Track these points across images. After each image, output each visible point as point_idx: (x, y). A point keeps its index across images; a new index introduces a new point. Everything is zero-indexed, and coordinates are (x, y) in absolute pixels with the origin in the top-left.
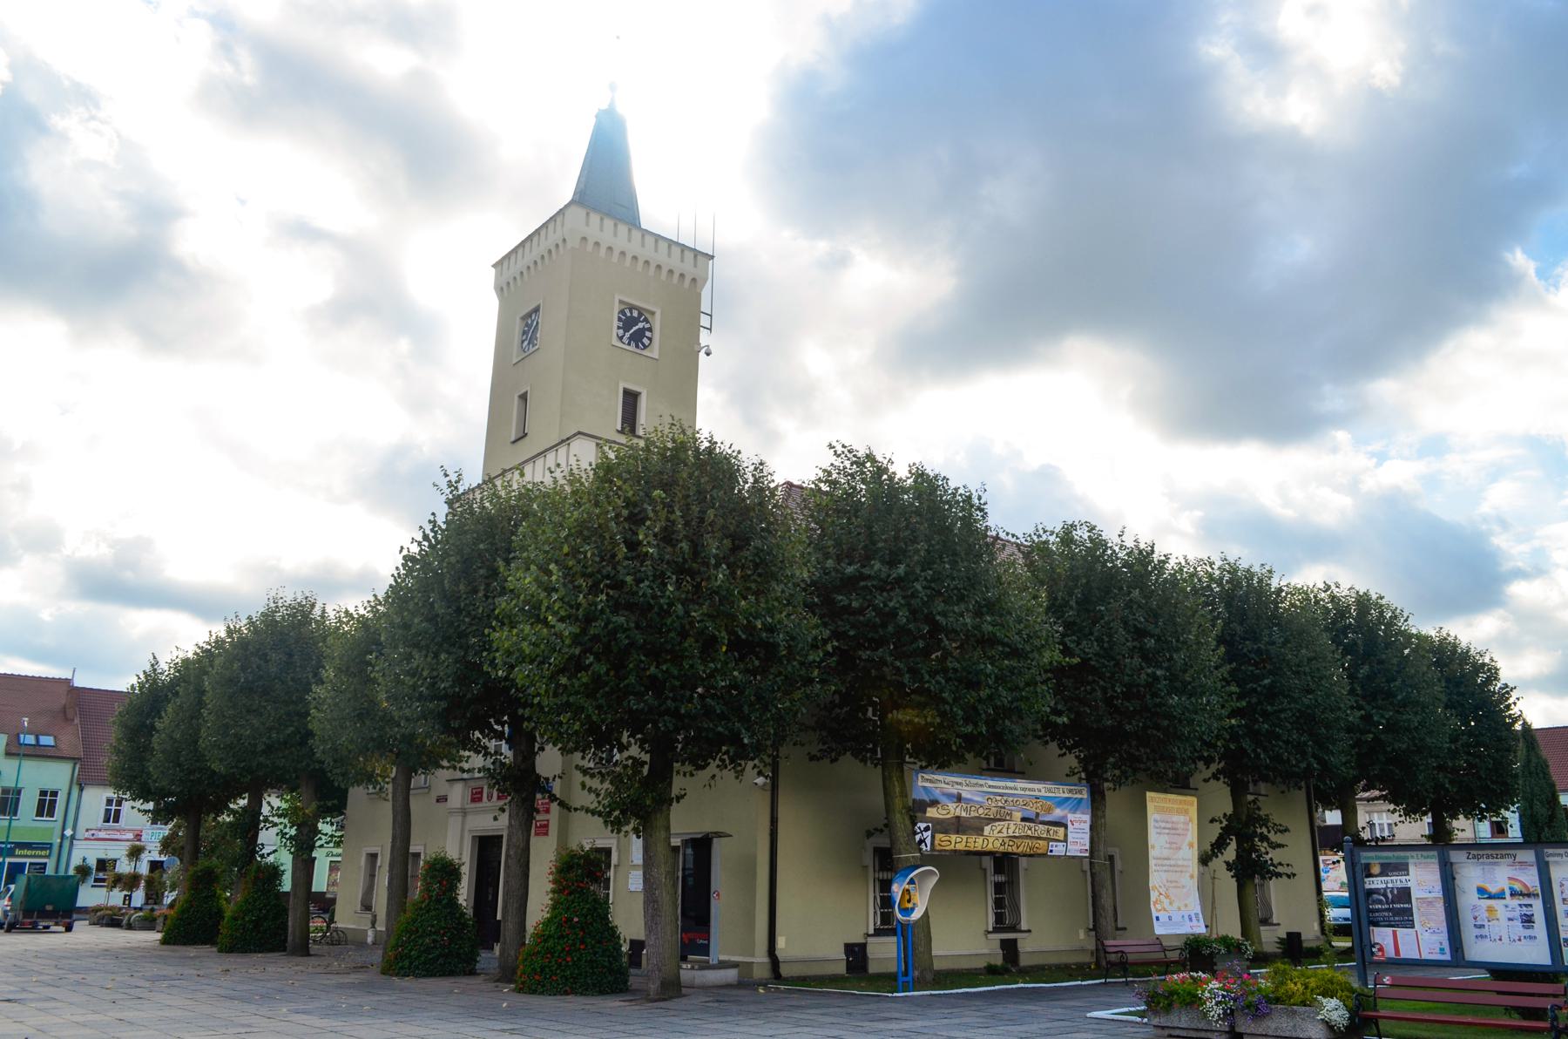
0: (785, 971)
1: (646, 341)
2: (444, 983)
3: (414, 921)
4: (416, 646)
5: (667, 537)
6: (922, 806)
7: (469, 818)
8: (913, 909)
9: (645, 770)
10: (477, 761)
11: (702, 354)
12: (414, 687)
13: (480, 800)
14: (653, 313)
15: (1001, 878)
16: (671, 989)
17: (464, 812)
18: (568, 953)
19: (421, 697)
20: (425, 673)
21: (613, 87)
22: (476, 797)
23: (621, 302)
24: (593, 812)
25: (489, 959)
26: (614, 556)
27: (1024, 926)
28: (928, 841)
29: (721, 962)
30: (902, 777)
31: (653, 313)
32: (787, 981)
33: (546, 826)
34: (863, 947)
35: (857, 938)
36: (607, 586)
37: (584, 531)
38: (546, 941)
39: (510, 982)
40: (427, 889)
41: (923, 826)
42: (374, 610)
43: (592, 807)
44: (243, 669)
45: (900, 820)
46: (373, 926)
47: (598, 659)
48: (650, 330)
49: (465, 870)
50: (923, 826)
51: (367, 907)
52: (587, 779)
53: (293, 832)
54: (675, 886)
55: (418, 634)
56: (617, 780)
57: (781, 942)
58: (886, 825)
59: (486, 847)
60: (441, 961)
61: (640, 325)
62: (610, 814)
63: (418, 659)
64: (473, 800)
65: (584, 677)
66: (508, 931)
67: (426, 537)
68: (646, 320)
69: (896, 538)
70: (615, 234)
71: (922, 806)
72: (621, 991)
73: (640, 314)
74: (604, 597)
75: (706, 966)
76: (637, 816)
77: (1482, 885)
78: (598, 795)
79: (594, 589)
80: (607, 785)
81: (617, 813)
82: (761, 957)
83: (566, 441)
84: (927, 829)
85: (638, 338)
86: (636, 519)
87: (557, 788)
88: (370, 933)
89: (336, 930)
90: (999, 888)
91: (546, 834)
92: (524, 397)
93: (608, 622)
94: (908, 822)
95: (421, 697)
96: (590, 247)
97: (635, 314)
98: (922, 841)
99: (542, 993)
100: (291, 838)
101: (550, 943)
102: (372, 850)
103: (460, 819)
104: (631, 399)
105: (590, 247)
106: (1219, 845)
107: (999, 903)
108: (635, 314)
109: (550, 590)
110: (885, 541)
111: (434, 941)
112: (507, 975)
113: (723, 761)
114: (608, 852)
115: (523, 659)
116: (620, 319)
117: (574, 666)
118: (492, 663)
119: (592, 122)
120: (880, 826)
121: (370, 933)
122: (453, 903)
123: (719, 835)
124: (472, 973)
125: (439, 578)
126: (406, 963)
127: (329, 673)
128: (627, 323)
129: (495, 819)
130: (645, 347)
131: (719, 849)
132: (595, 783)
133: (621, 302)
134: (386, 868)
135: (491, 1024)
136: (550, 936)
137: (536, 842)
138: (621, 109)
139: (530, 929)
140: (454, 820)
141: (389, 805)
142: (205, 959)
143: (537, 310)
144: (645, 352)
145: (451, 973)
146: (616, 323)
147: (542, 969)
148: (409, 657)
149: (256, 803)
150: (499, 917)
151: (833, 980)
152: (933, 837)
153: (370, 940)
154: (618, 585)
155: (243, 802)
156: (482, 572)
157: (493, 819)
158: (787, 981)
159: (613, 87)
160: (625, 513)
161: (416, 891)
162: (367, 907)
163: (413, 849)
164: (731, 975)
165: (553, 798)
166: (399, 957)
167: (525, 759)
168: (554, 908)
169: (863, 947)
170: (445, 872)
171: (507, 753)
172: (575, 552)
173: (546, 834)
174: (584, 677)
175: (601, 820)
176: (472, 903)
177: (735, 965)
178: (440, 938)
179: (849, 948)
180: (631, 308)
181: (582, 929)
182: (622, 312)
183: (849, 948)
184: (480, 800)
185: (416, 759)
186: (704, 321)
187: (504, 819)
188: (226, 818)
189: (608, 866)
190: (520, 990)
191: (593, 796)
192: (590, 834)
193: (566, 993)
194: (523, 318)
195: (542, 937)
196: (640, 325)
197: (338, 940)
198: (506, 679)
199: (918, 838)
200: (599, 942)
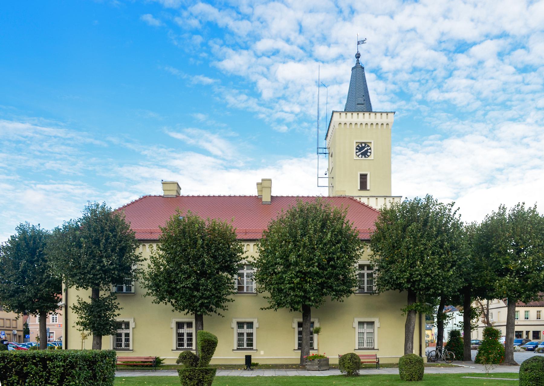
1: (369, 154)
13: (534, 332)
31: (371, 143)
48: (370, 149)
54: (459, 366)
61: (366, 149)
68: (368, 146)
70: (352, 118)
73: (365, 145)
85: (365, 154)
97: (363, 145)
104: (363, 177)
106: (31, 187)
108: (363, 145)
130: (368, 156)
133: (356, 143)
134: (298, 375)
146: (355, 151)
180: (361, 143)
184: (534, 332)
188: (435, 315)
196: (366, 149)
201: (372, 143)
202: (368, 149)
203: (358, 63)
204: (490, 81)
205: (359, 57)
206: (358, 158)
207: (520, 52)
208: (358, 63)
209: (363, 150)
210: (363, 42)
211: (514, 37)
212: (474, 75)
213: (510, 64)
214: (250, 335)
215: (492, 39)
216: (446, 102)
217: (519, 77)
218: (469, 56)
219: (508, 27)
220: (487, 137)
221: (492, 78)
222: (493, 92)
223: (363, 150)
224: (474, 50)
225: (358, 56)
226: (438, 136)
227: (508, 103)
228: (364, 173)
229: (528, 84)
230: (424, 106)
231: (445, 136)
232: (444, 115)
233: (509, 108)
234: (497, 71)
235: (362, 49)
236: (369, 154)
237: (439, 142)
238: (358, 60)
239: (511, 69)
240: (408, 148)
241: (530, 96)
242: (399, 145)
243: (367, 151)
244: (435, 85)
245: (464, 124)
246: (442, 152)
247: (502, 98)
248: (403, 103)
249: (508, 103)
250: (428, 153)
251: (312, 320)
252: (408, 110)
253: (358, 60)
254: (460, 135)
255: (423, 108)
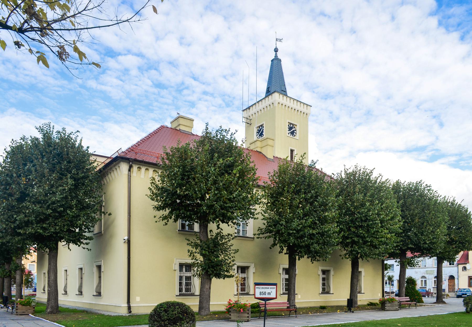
15: (324, 276)
27: (362, 292)
31: (296, 125)
48: (296, 130)
61: (293, 129)
68: (294, 128)
77: (264, 126)
85: (292, 133)
90: (324, 279)
107: (324, 285)
113: (67, 165)
128: (290, 129)
133: (289, 123)
138: (278, 47)
180: (291, 124)
196: (293, 129)
201: (298, 126)
202: (294, 130)
203: (276, 56)
204: (135, 87)
205: (277, 51)
206: (288, 135)
207: (153, 72)
208: (276, 56)
209: (292, 129)
210: (280, 40)
211: (148, 59)
212: (123, 78)
213: (149, 78)
214: (425, 281)
215: (132, 55)
216: (102, 92)
217: (156, 90)
218: (117, 61)
219: (144, 51)
220: (138, 128)
221: (136, 85)
222: (138, 95)
223: (292, 129)
224: (120, 58)
225: (276, 50)
226: (99, 118)
227: (150, 107)
228: (293, 148)
229: (162, 97)
230: (85, 90)
231: (105, 119)
232: (102, 102)
233: (152, 111)
234: (140, 80)
235: (279, 45)
236: (295, 134)
237: (101, 123)
238: (276, 54)
239: (150, 83)
240: (74, 121)
241: (166, 106)
242: (66, 117)
243: (294, 131)
244: (92, 76)
245: (119, 114)
246: (104, 132)
247: (146, 102)
248: (65, 82)
249: (150, 107)
250: (92, 130)
251: (360, 270)
252: (70, 90)
253: (276, 54)
254: (117, 122)
255: (83, 91)
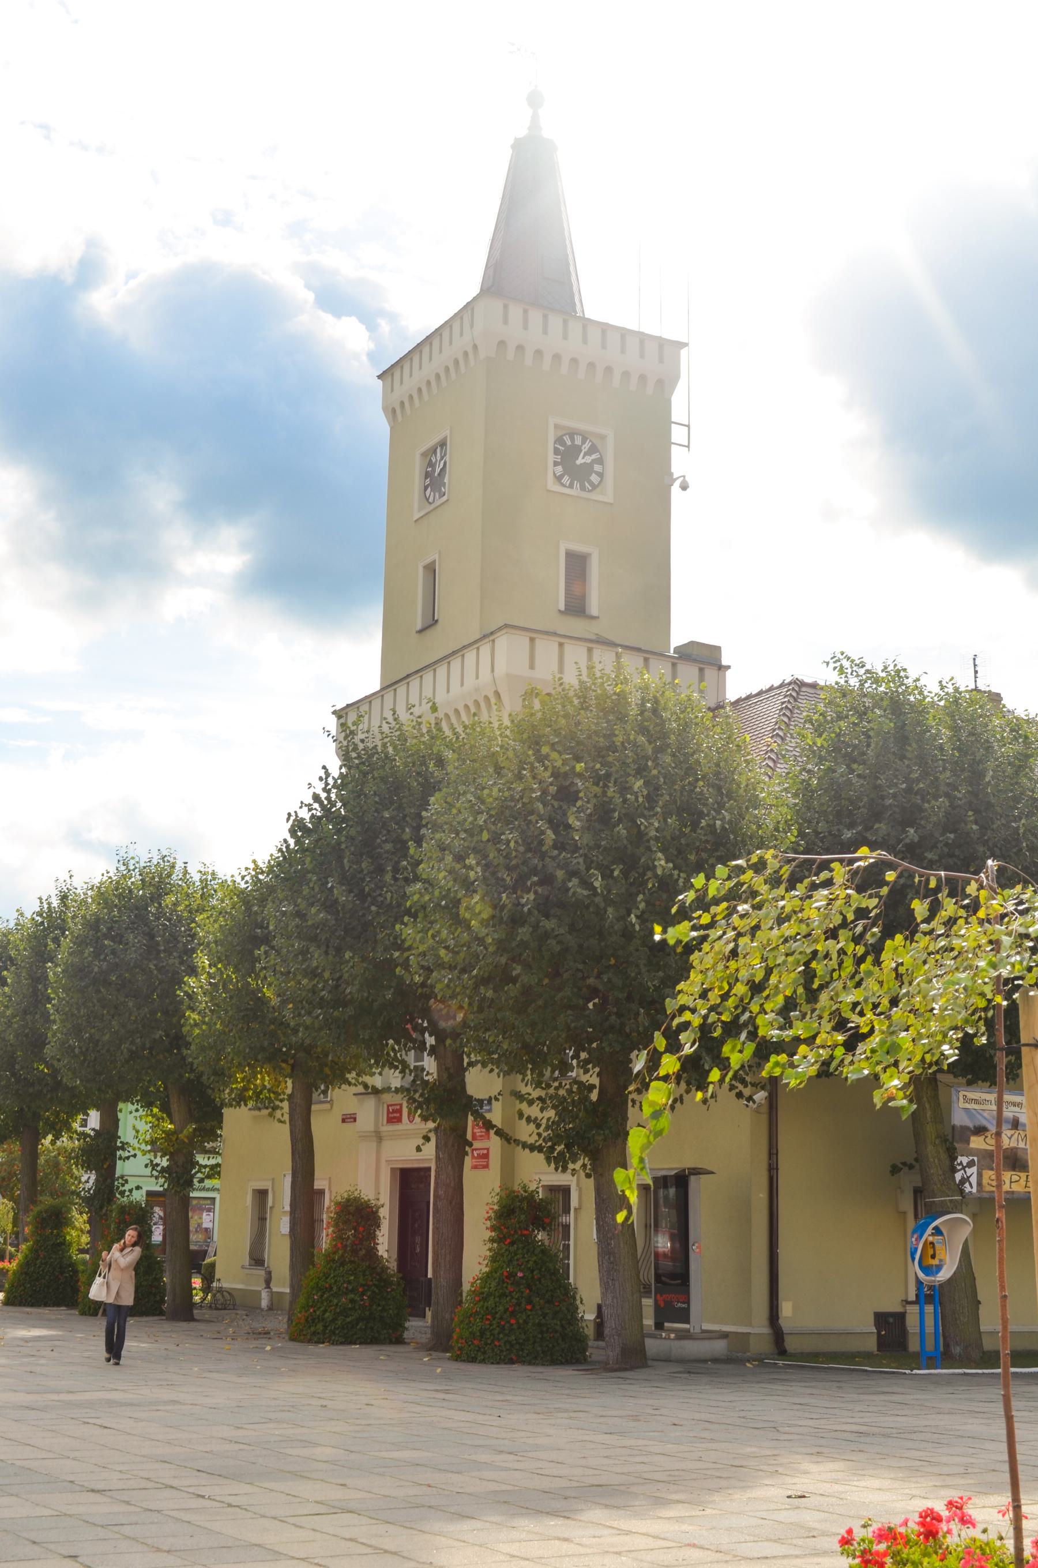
0: (791, 1344)
1: (594, 478)
2: (370, 1351)
3: (327, 1276)
4: (314, 939)
5: (603, 816)
6: (966, 1133)
7: (386, 1144)
8: (939, 1268)
9: (594, 1096)
10: (395, 1079)
11: (675, 489)
12: (314, 991)
13: (399, 1120)
14: (603, 438)
16: (632, 1360)
17: (379, 1137)
18: (513, 1313)
19: (322, 1003)
20: (327, 975)
21: (534, 100)
22: (394, 1117)
23: (556, 426)
24: (532, 1148)
25: (418, 1327)
26: (541, 843)
28: (974, 1180)
29: (704, 1331)
30: (935, 1097)
31: (603, 438)
32: (794, 1357)
33: (486, 1156)
34: (900, 1318)
35: (892, 1306)
36: (534, 884)
37: (510, 813)
38: (485, 1299)
39: (446, 1350)
40: (339, 1237)
41: (965, 1160)
42: (256, 881)
43: (531, 1140)
44: (96, 955)
45: (933, 1152)
46: (268, 1282)
47: (527, 966)
48: (600, 461)
49: (384, 1213)
50: (965, 1160)
51: (257, 1260)
52: (524, 1106)
53: (165, 1163)
55: (315, 926)
56: (560, 1105)
57: (786, 1309)
58: (916, 1160)
59: (409, 1182)
60: (361, 1325)
62: (552, 1149)
63: (317, 958)
64: (390, 1120)
65: (513, 990)
66: (440, 1293)
67: (316, 798)
69: (909, 790)
71: (966, 1133)
72: (578, 1362)
74: (532, 896)
75: (684, 1335)
76: (585, 1151)
78: (538, 1126)
79: (519, 885)
80: (551, 1113)
81: (560, 1148)
82: (759, 1327)
83: (488, 636)
84: (971, 1164)
86: (567, 795)
87: (496, 1115)
88: (265, 1295)
89: (220, 1290)
91: (486, 1166)
92: (431, 570)
93: (536, 927)
94: (944, 1156)
95: (322, 1003)
96: (510, 355)
98: (963, 1181)
99: (483, 1361)
100: (163, 1170)
101: (491, 1302)
102: (261, 1185)
103: (374, 1144)
105: (510, 355)
109: (469, 886)
110: (894, 796)
111: (352, 1301)
112: (441, 1343)
114: (566, 1191)
115: (441, 966)
116: (556, 451)
117: (501, 977)
118: (406, 965)
119: (505, 156)
120: (910, 1160)
121: (265, 1295)
122: (372, 1253)
123: (697, 1172)
124: (399, 1341)
125: (337, 851)
126: (320, 1327)
127: (203, 960)
129: (419, 1149)
130: (594, 487)
131: (700, 1191)
132: (534, 1111)
133: (556, 426)
135: (424, 1386)
136: (490, 1294)
137: (469, 1175)
139: (466, 1287)
140: (366, 1145)
141: (286, 1128)
142: (84, 1317)
143: (443, 444)
144: (594, 496)
145: (374, 1341)
146: (551, 457)
147: (482, 1333)
148: (304, 952)
149: (111, 1122)
150: (430, 1275)
151: (866, 1357)
152: (980, 1175)
153: (264, 1303)
154: (547, 880)
155: (94, 1119)
156: (388, 846)
157: (414, 1144)
158: (794, 1357)
159: (534, 100)
160: (553, 789)
161: (325, 1240)
162: (257, 1260)
163: (318, 1185)
164: (719, 1347)
165: (488, 1125)
166: (311, 1321)
167: (450, 1077)
168: (494, 1259)
169: (900, 1318)
170: (358, 1215)
171: (430, 1064)
172: (495, 839)
173: (486, 1166)
174: (513, 990)
175: (542, 1156)
176: (395, 1256)
177: (725, 1335)
178: (360, 1297)
179: (880, 1319)
181: (529, 1287)
182: (559, 440)
183: (880, 1319)
184: (399, 1120)
185: (313, 1072)
186: (677, 434)
187: (430, 1150)
189: (567, 1210)
190: (457, 1358)
191: (532, 1126)
192: (537, 1174)
193: (511, 1362)
194: (424, 455)
195: (481, 1295)
197: (226, 1304)
198: (423, 985)
199: (958, 1176)
200: (549, 1302)
